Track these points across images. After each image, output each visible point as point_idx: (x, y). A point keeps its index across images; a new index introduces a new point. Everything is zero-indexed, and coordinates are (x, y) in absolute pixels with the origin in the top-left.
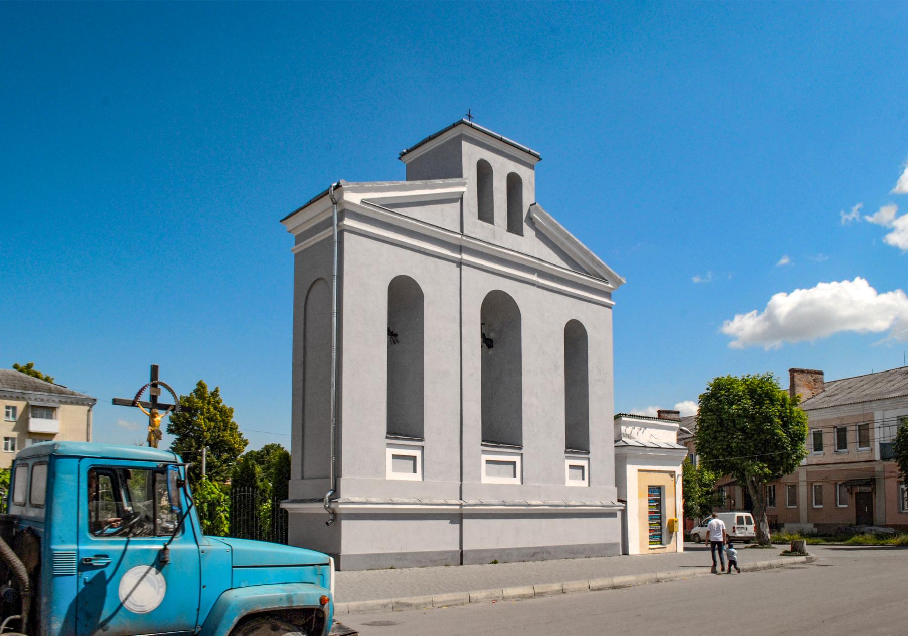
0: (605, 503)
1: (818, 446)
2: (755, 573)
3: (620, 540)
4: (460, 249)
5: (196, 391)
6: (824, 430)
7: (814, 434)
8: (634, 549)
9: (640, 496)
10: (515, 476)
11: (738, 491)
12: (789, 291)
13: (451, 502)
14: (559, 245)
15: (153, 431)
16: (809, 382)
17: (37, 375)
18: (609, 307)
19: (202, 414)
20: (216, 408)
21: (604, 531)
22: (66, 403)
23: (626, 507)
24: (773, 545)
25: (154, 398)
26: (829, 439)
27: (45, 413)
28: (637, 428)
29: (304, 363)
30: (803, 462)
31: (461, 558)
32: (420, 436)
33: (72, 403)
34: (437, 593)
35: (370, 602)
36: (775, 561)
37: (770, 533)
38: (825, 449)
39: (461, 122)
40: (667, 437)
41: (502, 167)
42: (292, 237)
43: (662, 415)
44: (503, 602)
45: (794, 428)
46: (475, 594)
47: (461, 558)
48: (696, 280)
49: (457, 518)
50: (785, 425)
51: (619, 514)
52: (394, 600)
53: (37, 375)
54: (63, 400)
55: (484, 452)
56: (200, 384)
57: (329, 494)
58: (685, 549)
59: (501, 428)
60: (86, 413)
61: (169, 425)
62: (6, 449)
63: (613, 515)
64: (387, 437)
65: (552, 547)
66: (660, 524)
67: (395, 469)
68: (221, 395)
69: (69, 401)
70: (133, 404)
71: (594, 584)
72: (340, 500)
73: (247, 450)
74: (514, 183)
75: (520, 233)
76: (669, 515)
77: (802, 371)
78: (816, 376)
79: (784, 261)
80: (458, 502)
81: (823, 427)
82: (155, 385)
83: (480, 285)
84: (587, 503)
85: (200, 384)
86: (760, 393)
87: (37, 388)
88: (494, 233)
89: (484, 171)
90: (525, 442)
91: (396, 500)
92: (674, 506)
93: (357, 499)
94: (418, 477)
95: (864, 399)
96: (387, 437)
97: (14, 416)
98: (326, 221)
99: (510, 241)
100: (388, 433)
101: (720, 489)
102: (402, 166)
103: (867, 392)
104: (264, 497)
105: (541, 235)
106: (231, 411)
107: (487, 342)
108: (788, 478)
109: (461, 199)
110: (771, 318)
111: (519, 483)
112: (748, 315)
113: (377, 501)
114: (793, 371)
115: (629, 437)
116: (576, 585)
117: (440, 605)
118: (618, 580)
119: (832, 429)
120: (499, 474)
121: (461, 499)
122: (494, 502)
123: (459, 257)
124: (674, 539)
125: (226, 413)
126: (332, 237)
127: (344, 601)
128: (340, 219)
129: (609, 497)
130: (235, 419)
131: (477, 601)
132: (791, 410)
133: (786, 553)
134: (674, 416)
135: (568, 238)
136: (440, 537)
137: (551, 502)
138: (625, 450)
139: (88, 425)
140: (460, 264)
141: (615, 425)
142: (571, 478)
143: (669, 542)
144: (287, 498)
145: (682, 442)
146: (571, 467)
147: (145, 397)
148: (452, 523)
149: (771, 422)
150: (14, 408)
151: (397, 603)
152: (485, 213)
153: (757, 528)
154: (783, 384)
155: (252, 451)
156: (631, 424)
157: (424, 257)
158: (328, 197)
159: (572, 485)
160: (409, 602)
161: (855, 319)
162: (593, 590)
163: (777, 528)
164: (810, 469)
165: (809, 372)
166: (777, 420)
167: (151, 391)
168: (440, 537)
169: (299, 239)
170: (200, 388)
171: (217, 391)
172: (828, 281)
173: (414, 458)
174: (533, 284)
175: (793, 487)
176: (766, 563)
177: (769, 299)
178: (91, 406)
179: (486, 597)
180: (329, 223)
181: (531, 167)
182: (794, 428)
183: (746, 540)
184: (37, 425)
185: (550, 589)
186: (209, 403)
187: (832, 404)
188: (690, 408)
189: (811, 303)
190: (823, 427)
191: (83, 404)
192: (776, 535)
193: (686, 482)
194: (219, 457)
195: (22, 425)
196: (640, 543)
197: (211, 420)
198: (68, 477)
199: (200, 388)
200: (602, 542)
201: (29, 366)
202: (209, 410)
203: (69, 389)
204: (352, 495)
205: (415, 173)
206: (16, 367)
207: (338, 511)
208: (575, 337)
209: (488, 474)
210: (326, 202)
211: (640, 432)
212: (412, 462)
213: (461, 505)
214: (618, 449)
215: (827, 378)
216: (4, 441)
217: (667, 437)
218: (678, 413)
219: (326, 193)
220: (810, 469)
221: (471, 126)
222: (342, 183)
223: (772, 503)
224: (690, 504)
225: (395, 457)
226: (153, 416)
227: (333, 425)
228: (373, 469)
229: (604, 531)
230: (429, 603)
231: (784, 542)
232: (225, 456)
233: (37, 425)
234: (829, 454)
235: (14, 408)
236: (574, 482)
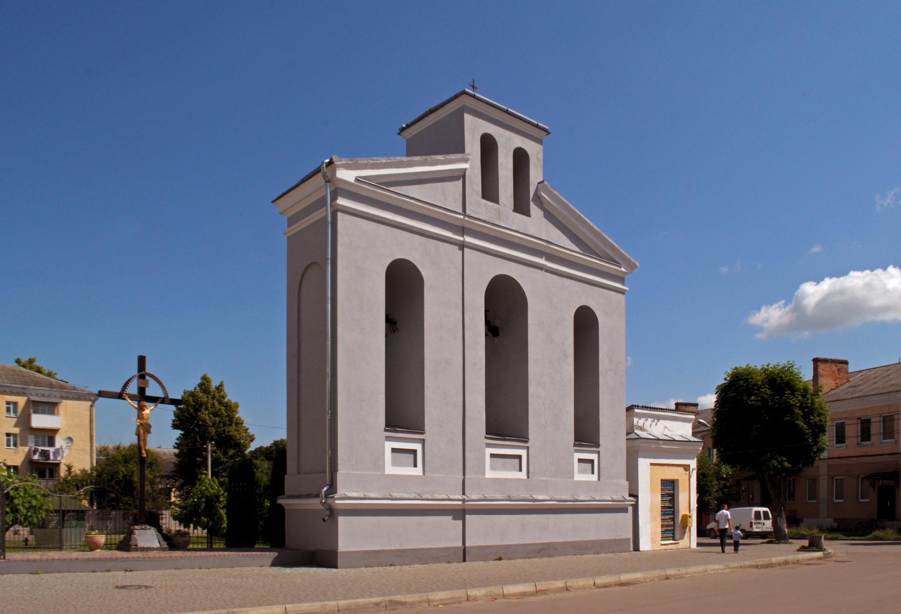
0: (615, 497)
1: (840, 438)
2: (769, 570)
3: (630, 535)
4: (463, 231)
5: (200, 385)
6: (847, 422)
7: (837, 426)
8: (645, 545)
9: (652, 491)
10: (521, 470)
11: (756, 485)
12: (818, 280)
13: (455, 498)
14: (569, 227)
15: (141, 424)
16: (833, 372)
17: (39, 371)
18: (622, 292)
19: (206, 409)
20: (221, 403)
21: (620, 526)
22: (67, 398)
23: (637, 502)
24: (791, 541)
25: (142, 390)
26: (853, 431)
27: (47, 408)
28: (650, 420)
29: (299, 352)
30: (824, 455)
31: (464, 554)
32: (420, 429)
33: (73, 399)
34: (433, 591)
35: (361, 601)
36: (790, 557)
37: (788, 527)
38: (847, 441)
39: (464, 93)
40: (682, 430)
41: (508, 142)
42: (284, 219)
43: (679, 407)
44: (503, 600)
45: (815, 419)
46: (473, 592)
47: (464, 554)
48: (724, 270)
49: (460, 513)
50: (806, 417)
51: (630, 509)
52: (387, 598)
53: (39, 371)
54: (64, 395)
55: (488, 445)
56: (205, 378)
57: (325, 489)
58: (699, 545)
59: (506, 420)
60: (88, 408)
61: (174, 421)
62: (8, 445)
63: (625, 510)
64: (385, 430)
66: (673, 519)
67: (395, 464)
68: (227, 389)
69: (70, 396)
70: (120, 396)
71: (599, 581)
72: (336, 496)
73: (253, 447)
74: (521, 159)
75: (527, 214)
76: (682, 510)
77: (825, 361)
78: (840, 366)
79: (816, 249)
80: (460, 497)
81: (846, 419)
82: (142, 377)
83: (484, 270)
84: (597, 498)
85: (205, 378)
86: (780, 383)
87: (37, 383)
88: (499, 214)
89: (488, 146)
91: (395, 495)
92: (688, 501)
93: (354, 495)
94: (418, 471)
95: (891, 390)
96: (385, 430)
97: (15, 412)
98: (318, 200)
99: (517, 221)
100: (387, 425)
101: (738, 483)
102: (402, 142)
103: (893, 382)
104: (243, 493)
105: (549, 216)
106: (237, 406)
107: (492, 330)
108: (808, 472)
109: (464, 177)
110: (799, 309)
112: (775, 306)
113: (376, 497)
114: (816, 361)
115: (642, 429)
116: (581, 582)
117: (435, 603)
118: (624, 577)
119: (856, 421)
120: (504, 468)
121: (464, 494)
122: (499, 497)
123: (461, 239)
124: (687, 534)
125: (231, 408)
126: (326, 217)
127: (335, 599)
128: (334, 199)
129: (621, 493)
130: (241, 414)
131: (475, 599)
132: (812, 400)
133: (803, 549)
134: (692, 408)
135: (579, 218)
136: (444, 533)
137: (558, 497)
138: (637, 442)
139: (91, 421)
140: (462, 246)
141: (627, 417)
142: (580, 472)
143: (682, 538)
144: (283, 494)
145: (700, 435)
146: (580, 461)
147: (133, 389)
148: (454, 519)
149: (792, 412)
150: (15, 404)
151: (391, 601)
152: (490, 192)
153: (774, 524)
154: (807, 375)
155: (261, 447)
156: (643, 416)
157: (424, 239)
158: (319, 175)
159: (582, 479)
160: (403, 600)
161: (886, 309)
162: (598, 587)
163: (796, 520)
164: (831, 462)
165: (834, 361)
166: (797, 411)
167: (139, 383)
168: (444, 533)
169: (292, 221)
170: (205, 384)
171: (221, 385)
172: (862, 269)
173: (414, 452)
175: (814, 482)
176: (781, 559)
177: (797, 287)
178: (93, 402)
179: (486, 595)
180: (322, 203)
181: (539, 141)
182: (815, 419)
183: (763, 535)
184: (39, 421)
185: (552, 587)
186: (213, 398)
187: (856, 395)
188: (709, 401)
189: (842, 292)
190: (846, 419)
191: (85, 400)
192: (794, 530)
193: (701, 477)
194: (225, 453)
195: (24, 421)
196: (652, 539)
197: (215, 414)
199: (205, 384)
200: (613, 538)
201: (31, 361)
202: (213, 404)
203: (72, 383)
204: (349, 489)
205: (419, 148)
206: (18, 361)
207: (335, 507)
208: (585, 324)
210: (319, 179)
211: (654, 424)
212: (412, 456)
213: (464, 500)
214: (630, 442)
215: (851, 368)
216: (5, 438)
217: (682, 430)
218: (696, 405)
219: (318, 171)
220: (831, 462)
221: (474, 96)
222: (334, 159)
223: (792, 496)
224: (706, 498)
225: (394, 450)
226: (141, 409)
227: (328, 417)
228: (371, 464)
229: (620, 526)
230: (425, 601)
231: (802, 537)
232: (231, 452)
233: (39, 421)
234: (852, 446)
235: (15, 404)
236: (582, 476)
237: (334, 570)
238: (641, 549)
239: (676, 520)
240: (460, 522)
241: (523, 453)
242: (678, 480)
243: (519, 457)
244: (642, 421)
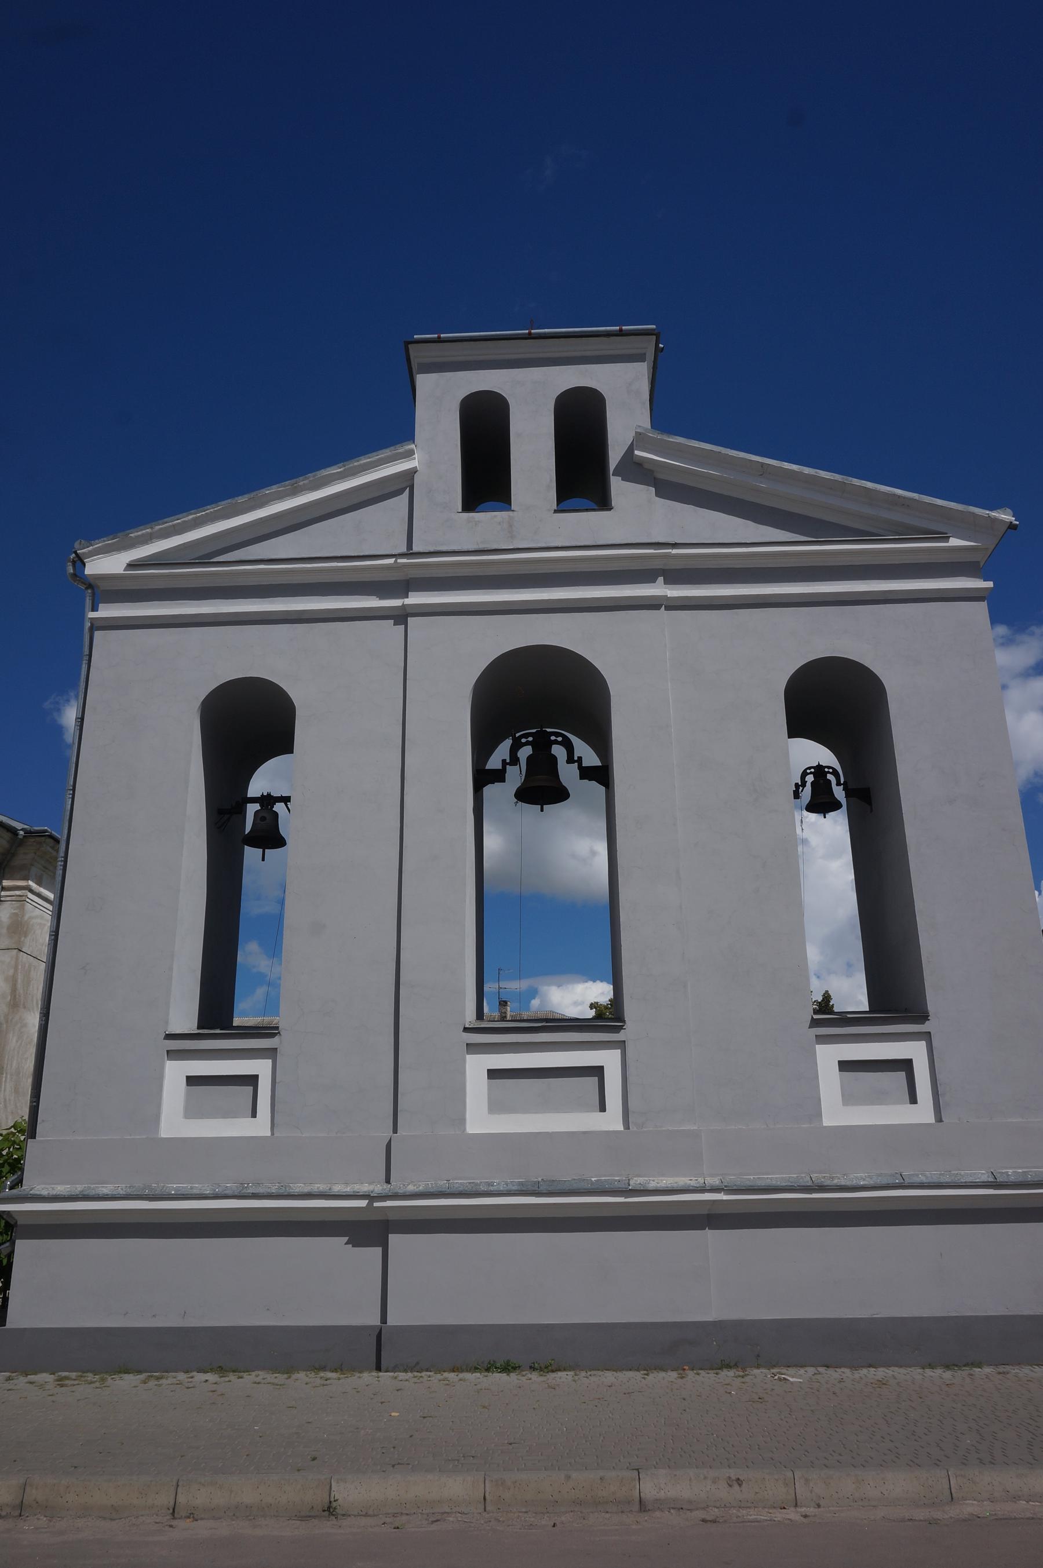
10: (913, 1100)
49: (370, 1230)
67: (849, 1098)
93: (61, 1189)
99: (585, 526)
111: (929, 1118)
120: (545, 1106)
140: (401, 617)
212: (902, 1075)
225: (845, 1066)
240: (378, 1251)
243: (906, 1065)
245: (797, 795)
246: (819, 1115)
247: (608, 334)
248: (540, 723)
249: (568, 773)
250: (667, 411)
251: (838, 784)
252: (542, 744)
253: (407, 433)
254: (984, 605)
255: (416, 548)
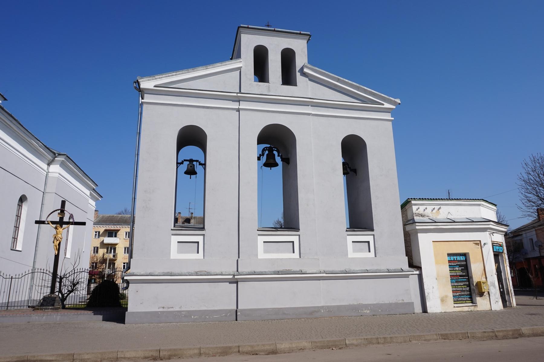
10: (370, 251)
65: (334, 307)
66: (469, 286)
67: (354, 251)
90: (301, 226)
99: (288, 90)
111: (374, 256)
120: (278, 251)
140: (238, 110)
174: (309, 114)
198: (44, 267)
208: (353, 152)
209: (354, 251)
237: (122, 325)
238: (429, 311)
239: (471, 285)
241: (295, 239)
242: (468, 253)
244: (422, 208)
245: (259, 159)
246: (347, 255)
247: (297, 34)
248: (277, 146)
249: (278, 160)
250: (312, 60)
251: (278, 156)
252: (270, 150)
253: (239, 56)
254: (391, 123)
255: (242, 92)
